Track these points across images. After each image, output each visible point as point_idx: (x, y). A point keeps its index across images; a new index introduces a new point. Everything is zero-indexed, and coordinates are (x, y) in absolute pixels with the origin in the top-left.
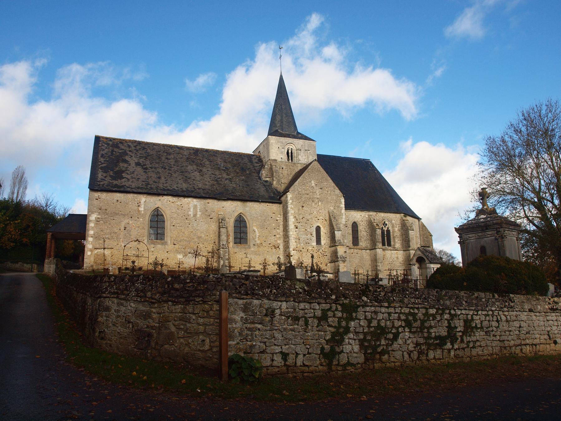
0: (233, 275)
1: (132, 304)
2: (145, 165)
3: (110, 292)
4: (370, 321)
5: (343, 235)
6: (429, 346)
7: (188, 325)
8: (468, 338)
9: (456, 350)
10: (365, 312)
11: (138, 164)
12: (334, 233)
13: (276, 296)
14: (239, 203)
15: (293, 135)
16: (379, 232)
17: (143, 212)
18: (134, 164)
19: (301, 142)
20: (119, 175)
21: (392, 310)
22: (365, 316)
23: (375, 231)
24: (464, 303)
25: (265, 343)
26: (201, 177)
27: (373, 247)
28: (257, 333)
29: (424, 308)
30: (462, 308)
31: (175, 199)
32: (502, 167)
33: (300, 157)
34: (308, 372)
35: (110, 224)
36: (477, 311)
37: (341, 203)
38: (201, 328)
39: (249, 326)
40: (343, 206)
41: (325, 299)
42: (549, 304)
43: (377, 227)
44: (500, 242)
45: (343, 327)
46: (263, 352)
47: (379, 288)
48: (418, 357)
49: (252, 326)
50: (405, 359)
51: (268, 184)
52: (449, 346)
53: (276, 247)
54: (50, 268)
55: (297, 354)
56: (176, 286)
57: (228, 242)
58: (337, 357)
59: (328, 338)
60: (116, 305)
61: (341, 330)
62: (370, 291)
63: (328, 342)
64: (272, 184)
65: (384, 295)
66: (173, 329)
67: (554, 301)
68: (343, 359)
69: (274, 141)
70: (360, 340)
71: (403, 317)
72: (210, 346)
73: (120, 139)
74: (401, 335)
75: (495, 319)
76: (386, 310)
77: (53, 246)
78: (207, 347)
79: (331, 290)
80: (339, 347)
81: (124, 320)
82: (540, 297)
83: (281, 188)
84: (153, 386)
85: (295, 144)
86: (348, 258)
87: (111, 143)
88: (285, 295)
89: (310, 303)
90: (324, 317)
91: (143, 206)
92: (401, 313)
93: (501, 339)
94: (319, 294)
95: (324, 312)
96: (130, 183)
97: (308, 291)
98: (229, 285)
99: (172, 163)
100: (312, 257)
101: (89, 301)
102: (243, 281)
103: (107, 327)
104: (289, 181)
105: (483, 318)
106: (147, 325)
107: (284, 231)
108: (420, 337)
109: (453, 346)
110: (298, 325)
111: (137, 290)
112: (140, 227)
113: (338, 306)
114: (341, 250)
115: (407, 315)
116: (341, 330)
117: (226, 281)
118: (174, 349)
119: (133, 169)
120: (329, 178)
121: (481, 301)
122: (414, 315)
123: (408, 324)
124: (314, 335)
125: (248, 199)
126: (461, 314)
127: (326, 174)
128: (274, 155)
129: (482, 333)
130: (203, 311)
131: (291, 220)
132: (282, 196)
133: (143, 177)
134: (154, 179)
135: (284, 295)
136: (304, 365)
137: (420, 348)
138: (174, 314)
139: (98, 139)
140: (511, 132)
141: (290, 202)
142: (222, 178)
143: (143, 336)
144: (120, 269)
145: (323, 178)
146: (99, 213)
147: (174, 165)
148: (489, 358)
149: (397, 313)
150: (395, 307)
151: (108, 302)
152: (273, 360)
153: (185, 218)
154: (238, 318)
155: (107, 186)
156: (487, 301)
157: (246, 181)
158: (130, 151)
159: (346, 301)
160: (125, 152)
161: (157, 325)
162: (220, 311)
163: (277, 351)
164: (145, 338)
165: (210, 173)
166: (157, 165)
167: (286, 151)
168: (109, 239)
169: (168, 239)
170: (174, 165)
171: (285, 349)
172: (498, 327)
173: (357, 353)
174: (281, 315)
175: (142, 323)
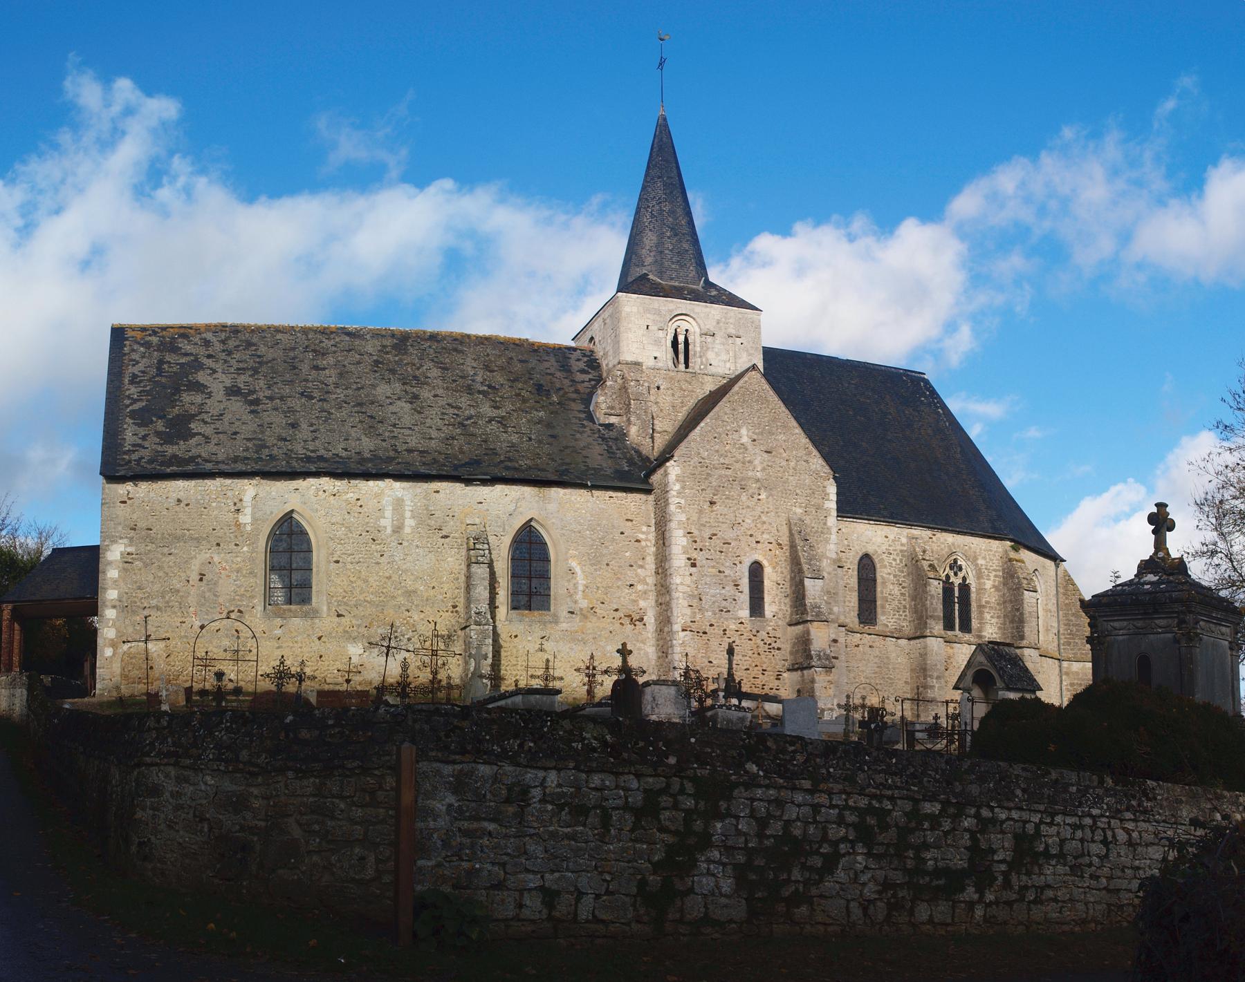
1: (208, 778)
2: (254, 392)
4: (763, 823)
5: (833, 591)
8: (1024, 878)
9: (990, 904)
10: (752, 800)
11: (233, 391)
12: (802, 583)
15: (692, 292)
16: (936, 588)
17: (249, 528)
18: (222, 392)
19: (716, 310)
20: (179, 429)
21: (823, 799)
22: (753, 810)
23: (925, 585)
24: (1019, 792)
25: (503, 865)
26: (417, 416)
28: (485, 841)
31: (340, 484)
33: (711, 355)
34: (605, 937)
36: (1053, 815)
37: (825, 496)
40: (832, 505)
46: (500, 886)
49: (475, 825)
51: (613, 434)
52: (970, 893)
53: (636, 620)
55: (580, 894)
56: (304, 734)
58: (679, 903)
61: (692, 841)
62: (768, 749)
63: (657, 867)
66: (297, 833)
69: (635, 309)
71: (851, 818)
75: (1099, 836)
78: (370, 873)
81: (191, 816)
82: (1226, 793)
85: (701, 318)
86: (842, 658)
87: (155, 340)
89: (617, 774)
90: (647, 810)
91: (248, 511)
92: (847, 807)
93: (1111, 887)
95: (651, 796)
96: (211, 448)
99: (331, 380)
100: (731, 652)
102: (455, 722)
104: (677, 424)
108: (895, 869)
109: (982, 896)
110: (584, 825)
112: (243, 568)
114: (820, 636)
119: (216, 401)
120: (794, 423)
121: (1066, 790)
122: (882, 814)
123: (864, 835)
126: (1008, 819)
127: (783, 408)
133: (249, 426)
134: (278, 430)
136: (597, 920)
137: (894, 896)
142: (479, 416)
145: (774, 420)
146: (131, 539)
147: (337, 385)
149: (837, 806)
150: (830, 793)
152: (520, 906)
154: (440, 807)
155: (151, 462)
156: (1083, 792)
157: (549, 425)
158: (209, 356)
160: (196, 360)
161: (263, 824)
162: (397, 790)
165: (441, 402)
167: (670, 338)
168: (158, 608)
169: (319, 599)
170: (337, 385)
172: (1107, 856)
174: (543, 801)
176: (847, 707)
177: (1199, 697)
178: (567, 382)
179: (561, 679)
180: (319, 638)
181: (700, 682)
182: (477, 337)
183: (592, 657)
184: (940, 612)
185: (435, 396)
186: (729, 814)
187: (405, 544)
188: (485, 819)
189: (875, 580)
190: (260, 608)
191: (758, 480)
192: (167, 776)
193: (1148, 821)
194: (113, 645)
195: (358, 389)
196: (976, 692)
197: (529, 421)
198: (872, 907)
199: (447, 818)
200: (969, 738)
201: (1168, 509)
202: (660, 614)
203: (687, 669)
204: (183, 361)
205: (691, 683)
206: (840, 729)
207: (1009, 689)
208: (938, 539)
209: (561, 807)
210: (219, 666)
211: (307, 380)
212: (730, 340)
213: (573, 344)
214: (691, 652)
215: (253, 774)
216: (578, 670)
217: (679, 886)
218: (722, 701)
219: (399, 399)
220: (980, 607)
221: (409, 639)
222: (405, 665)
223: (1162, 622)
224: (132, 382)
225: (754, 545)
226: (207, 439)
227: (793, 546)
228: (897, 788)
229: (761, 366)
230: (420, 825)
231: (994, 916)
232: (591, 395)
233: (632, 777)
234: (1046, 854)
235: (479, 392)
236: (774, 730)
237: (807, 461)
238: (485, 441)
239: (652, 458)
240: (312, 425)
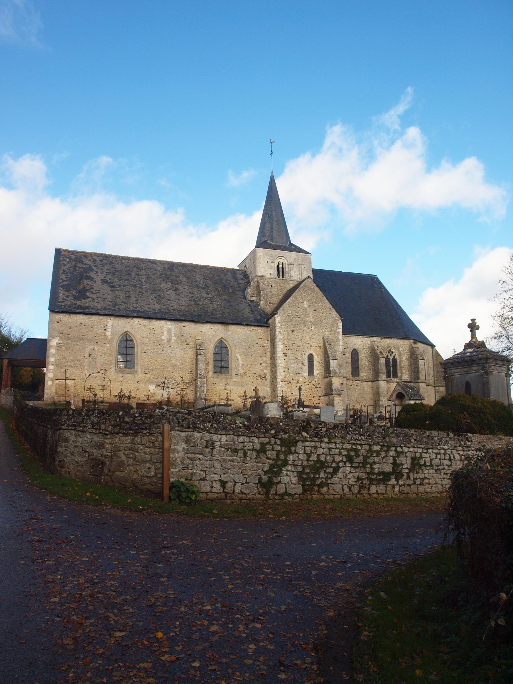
0: (177, 410)
1: (88, 435)
3: (68, 425)
4: (309, 456)
5: (339, 364)
6: (372, 482)
7: (137, 454)
8: (415, 475)
10: (305, 446)
11: (104, 281)
13: (216, 429)
15: (284, 247)
16: (382, 361)
17: (110, 337)
18: (100, 281)
19: (294, 255)
20: (82, 294)
21: (333, 445)
22: (305, 451)
23: (378, 360)
24: (413, 441)
25: (205, 471)
26: (177, 296)
27: (376, 378)
28: (198, 462)
29: (367, 444)
30: (410, 446)
31: (146, 322)
33: (292, 272)
35: (73, 350)
36: (427, 449)
37: (338, 327)
38: (148, 457)
39: (190, 456)
40: (340, 330)
41: (264, 434)
43: (381, 356)
44: (485, 379)
45: (282, 460)
46: (203, 479)
47: (321, 424)
48: (360, 491)
49: (194, 456)
50: (345, 492)
51: (254, 304)
52: (393, 481)
56: (127, 419)
58: (275, 487)
59: (266, 469)
60: (73, 436)
61: (280, 462)
62: (311, 427)
63: (266, 473)
64: (259, 305)
65: (326, 432)
66: (123, 458)
68: (281, 488)
69: (262, 255)
70: (298, 472)
71: (344, 453)
72: (155, 473)
73: (84, 253)
74: (341, 470)
75: (447, 457)
76: (327, 445)
78: (152, 474)
79: (271, 425)
80: (276, 477)
81: (81, 450)
83: (268, 309)
84: (103, 503)
85: (287, 258)
87: (73, 256)
88: (225, 429)
89: (249, 437)
90: (262, 450)
91: (110, 330)
92: (342, 448)
94: (259, 429)
96: (95, 303)
97: (247, 426)
98: (173, 419)
99: (143, 280)
100: (300, 389)
101: (50, 433)
102: (186, 416)
103: (66, 456)
104: (279, 300)
105: (434, 456)
106: (101, 454)
107: (271, 359)
108: (362, 472)
109: (398, 482)
110: (237, 456)
111: (92, 423)
112: (107, 354)
113: (277, 440)
114: (336, 382)
115: (349, 450)
116: (280, 462)
117: (170, 416)
118: (124, 476)
119: (100, 291)
120: (325, 299)
122: (356, 451)
123: (350, 459)
124: (253, 466)
125: (231, 322)
126: (409, 451)
127: (321, 293)
129: (431, 471)
130: (150, 442)
132: (270, 318)
134: (122, 299)
135: (224, 428)
136: (242, 493)
137: (362, 483)
138: (125, 444)
139: (58, 252)
141: (278, 325)
142: (201, 297)
143: (98, 464)
144: (83, 401)
145: (317, 298)
146: (61, 337)
147: (146, 282)
148: (439, 495)
149: (339, 448)
150: (336, 443)
151: (67, 434)
152: (212, 487)
153: (157, 343)
154: (180, 449)
155: (69, 307)
157: (228, 301)
158: (95, 266)
159: (286, 436)
160: (90, 267)
161: (110, 454)
162: (163, 441)
163: (216, 479)
164: (99, 465)
167: (276, 266)
168: (71, 367)
169: (138, 367)
170: (146, 282)
171: (224, 477)
172: (451, 465)
173: (295, 484)
174: (221, 447)
175: (96, 453)
177: (492, 398)
178: (235, 283)
179: (233, 400)
180: (138, 382)
182: (201, 266)
183: (245, 392)
184: (384, 371)
185: (184, 289)
186: (295, 452)
187: (172, 346)
188: (197, 454)
190: (113, 369)
191: (311, 322)
194: (52, 380)
195: (155, 284)
196: (397, 402)
197: (220, 299)
198: (353, 487)
199: (183, 453)
200: (394, 420)
201: (476, 321)
202: (272, 375)
203: (282, 397)
206: (344, 418)
207: (410, 400)
208: (383, 342)
209: (227, 449)
210: (96, 392)
211: (134, 280)
212: (300, 266)
213: (238, 268)
214: (284, 390)
215: (106, 435)
217: (275, 480)
219: (170, 289)
220: (401, 367)
221: (173, 384)
222: (169, 394)
223: (475, 368)
224: (63, 273)
225: (310, 347)
227: (325, 347)
228: (363, 440)
231: (403, 491)
233: (255, 438)
234: (425, 465)
235: (202, 288)
236: (317, 420)
237: (330, 313)
238: (204, 307)
239: (269, 314)
240: (135, 298)
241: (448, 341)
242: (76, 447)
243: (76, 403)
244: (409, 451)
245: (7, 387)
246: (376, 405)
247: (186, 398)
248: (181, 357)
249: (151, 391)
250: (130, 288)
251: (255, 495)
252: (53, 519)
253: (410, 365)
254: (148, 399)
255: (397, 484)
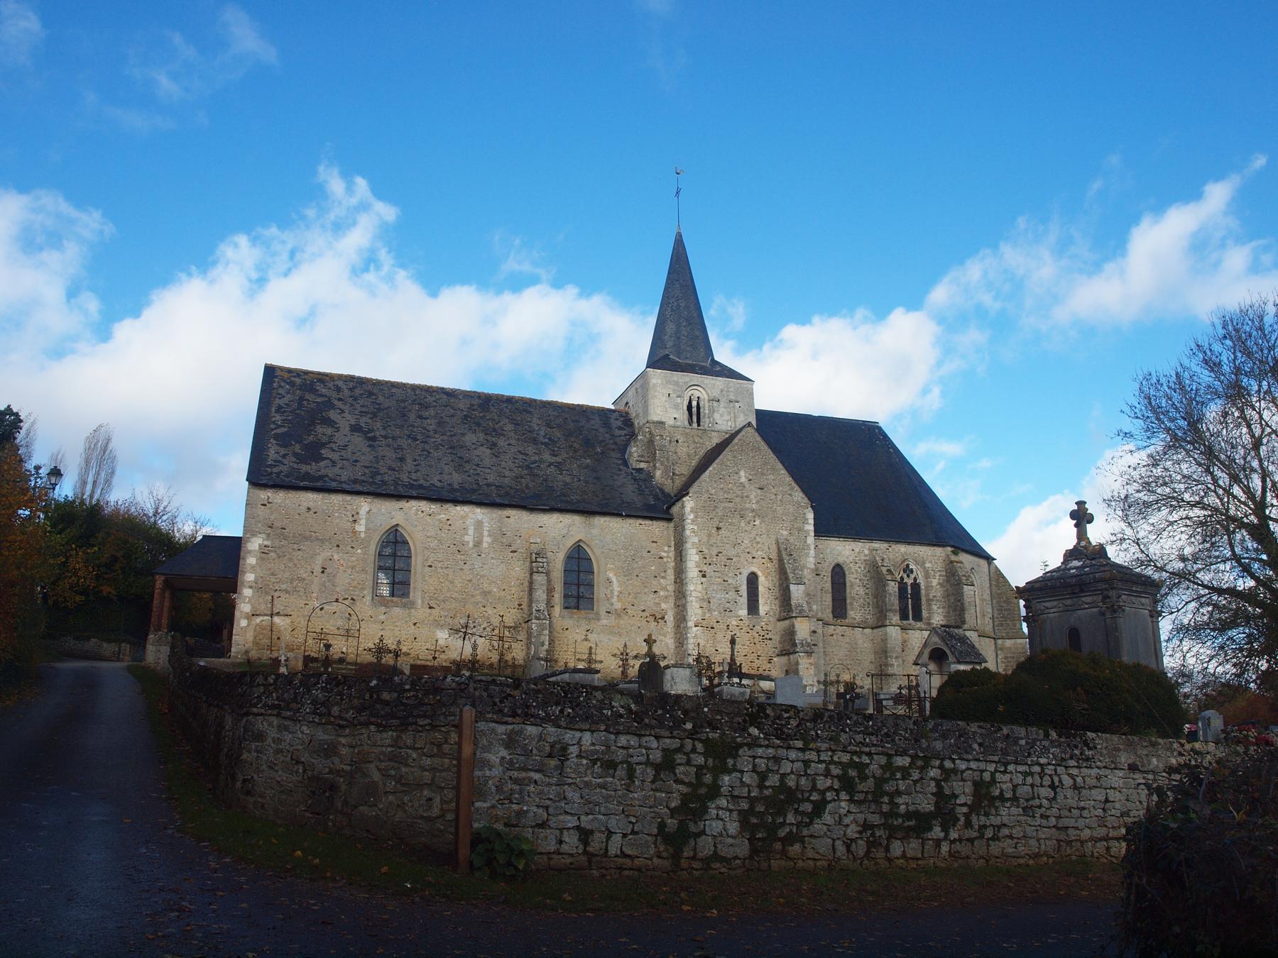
0: (490, 679)
1: (304, 728)
3: (265, 705)
4: (763, 777)
6: (893, 833)
8: (982, 818)
10: (754, 757)
11: (356, 428)
12: (788, 588)
14: (577, 519)
16: (893, 587)
17: (363, 535)
19: (720, 382)
20: (313, 452)
21: (812, 756)
22: (754, 766)
24: (976, 746)
25: (547, 808)
26: (494, 459)
27: (880, 624)
28: (531, 788)
30: (970, 757)
31: (434, 507)
32: (1175, 443)
33: (716, 416)
35: (290, 560)
36: (1006, 764)
37: (805, 521)
39: (515, 774)
40: (810, 527)
41: (671, 729)
42: (1180, 754)
45: (707, 786)
46: (543, 825)
48: (868, 852)
49: (523, 775)
50: (838, 854)
51: (643, 476)
52: (937, 832)
53: (659, 618)
54: (157, 652)
55: (610, 833)
56: (386, 696)
57: (550, 606)
58: (692, 842)
61: (703, 791)
62: (767, 716)
63: (673, 812)
66: (376, 776)
67: (1192, 750)
70: (740, 812)
71: (836, 771)
72: (442, 809)
73: (319, 374)
74: (829, 807)
77: (167, 604)
78: (435, 812)
79: (686, 712)
80: (695, 823)
81: (288, 759)
82: (1160, 740)
83: (670, 487)
85: (705, 388)
86: (821, 645)
87: (298, 381)
89: (640, 736)
90: (666, 765)
91: (363, 522)
92: (832, 762)
94: (660, 721)
96: (337, 470)
97: (636, 713)
98: (481, 696)
99: (431, 428)
100: (733, 642)
104: (691, 469)
105: (1019, 779)
110: (613, 777)
111: (314, 702)
112: (355, 567)
114: (803, 629)
116: (703, 791)
117: (475, 689)
119: (345, 442)
121: (1016, 743)
122: (861, 767)
123: (847, 784)
126: (968, 769)
128: (659, 411)
129: (1014, 810)
130: (432, 743)
131: (692, 558)
133: (366, 459)
137: (873, 835)
140: (1195, 365)
142: (541, 461)
143: (322, 790)
145: (765, 464)
146: (268, 535)
148: (1031, 862)
150: (818, 751)
151: (261, 724)
152: (561, 842)
154: (494, 759)
155: (287, 476)
157: (594, 470)
158: (340, 399)
159: (715, 735)
161: (347, 768)
162: (459, 744)
163: (570, 825)
165: (513, 450)
166: (397, 432)
167: (686, 403)
168: (287, 592)
169: (416, 595)
170: (435, 432)
171: (586, 821)
172: (1054, 798)
174: (579, 756)
175: (321, 765)
176: (826, 683)
181: (710, 665)
186: (735, 769)
189: (845, 584)
190: (369, 598)
191: (753, 511)
192: (270, 724)
193: (1091, 767)
196: (932, 667)
200: (928, 705)
204: (319, 400)
205: (702, 666)
207: (959, 662)
209: (594, 762)
215: (341, 726)
216: (614, 655)
217: (692, 828)
218: (726, 680)
220: (928, 600)
222: (475, 647)
223: (1088, 599)
224: (277, 411)
226: (334, 463)
227: (781, 560)
229: (754, 423)
230: (478, 773)
232: (626, 445)
234: (1001, 797)
238: (546, 480)
241: (1027, 545)
242: (279, 751)
243: (291, 661)
244: (968, 769)
245: (158, 629)
246: (881, 674)
247: (508, 657)
248: (503, 576)
249: (441, 642)
250: (403, 442)
251: (651, 859)
252: (214, 911)
253: (947, 596)
254: (435, 658)
255: (946, 838)
